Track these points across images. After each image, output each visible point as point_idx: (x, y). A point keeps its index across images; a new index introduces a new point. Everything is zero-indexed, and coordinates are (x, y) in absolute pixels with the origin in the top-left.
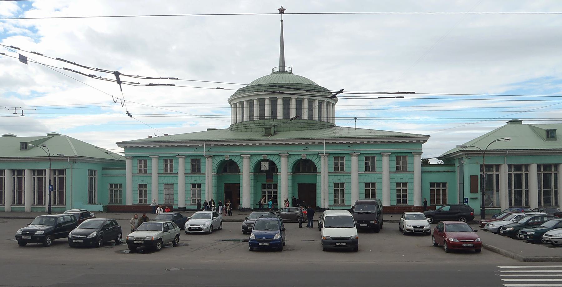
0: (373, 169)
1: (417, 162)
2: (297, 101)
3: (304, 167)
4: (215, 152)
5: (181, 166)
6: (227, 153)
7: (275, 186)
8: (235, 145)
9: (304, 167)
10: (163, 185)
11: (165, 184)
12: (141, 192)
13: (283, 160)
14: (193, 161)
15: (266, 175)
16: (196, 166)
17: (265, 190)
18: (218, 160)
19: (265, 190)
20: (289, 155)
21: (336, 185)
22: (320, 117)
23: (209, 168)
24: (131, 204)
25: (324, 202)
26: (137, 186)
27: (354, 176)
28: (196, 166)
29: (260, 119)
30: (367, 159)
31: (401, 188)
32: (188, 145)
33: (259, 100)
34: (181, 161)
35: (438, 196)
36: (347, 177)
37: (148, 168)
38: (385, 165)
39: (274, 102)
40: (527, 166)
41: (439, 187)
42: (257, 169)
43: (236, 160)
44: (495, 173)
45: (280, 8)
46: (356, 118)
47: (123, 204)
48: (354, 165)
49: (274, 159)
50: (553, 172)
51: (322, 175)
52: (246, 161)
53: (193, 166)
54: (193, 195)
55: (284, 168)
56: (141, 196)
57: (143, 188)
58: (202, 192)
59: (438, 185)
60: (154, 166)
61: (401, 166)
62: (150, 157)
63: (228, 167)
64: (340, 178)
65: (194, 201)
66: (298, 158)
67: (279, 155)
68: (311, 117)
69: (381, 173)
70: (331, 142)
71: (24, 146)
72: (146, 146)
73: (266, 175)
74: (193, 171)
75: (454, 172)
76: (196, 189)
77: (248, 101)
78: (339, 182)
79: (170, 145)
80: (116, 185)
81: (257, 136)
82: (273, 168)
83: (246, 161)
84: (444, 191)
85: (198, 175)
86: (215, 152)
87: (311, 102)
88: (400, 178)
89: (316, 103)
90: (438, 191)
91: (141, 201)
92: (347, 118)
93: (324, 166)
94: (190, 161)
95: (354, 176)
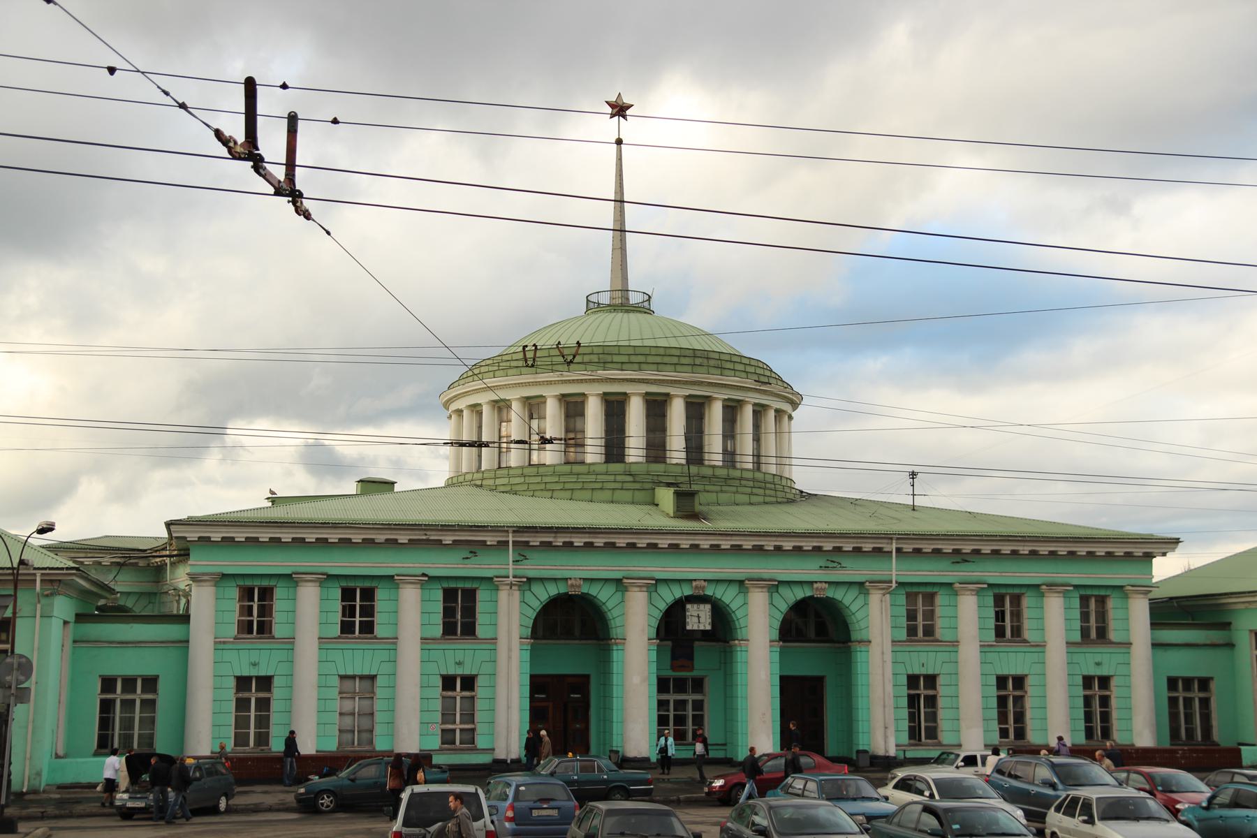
0: (1017, 631)
1: (1140, 611)
2: (724, 407)
3: (816, 625)
4: (537, 565)
5: (410, 614)
6: (576, 571)
7: (663, 685)
8: (674, 547)
9: (816, 625)
10: (335, 681)
11: (342, 677)
12: (242, 705)
14: (449, 595)
15: (693, 647)
16: (459, 612)
17: (664, 697)
19: (664, 697)
20: (775, 586)
21: (913, 680)
22: (757, 456)
23: (508, 617)
24: (314, 752)
25: (886, 737)
26: (232, 683)
27: (970, 653)
28: (459, 612)
29: (689, 461)
30: (347, 594)
31: (923, 692)
32: (448, 539)
35: (1189, 718)
36: (945, 656)
37: (992, 623)
38: (1054, 620)
41: (917, 688)
42: (671, 627)
43: (604, 595)
45: (613, 99)
46: (913, 475)
47: (381, 745)
48: (967, 617)
49: (727, 596)
51: (875, 649)
53: (448, 612)
54: (447, 716)
55: (758, 621)
56: (241, 723)
57: (254, 692)
58: (479, 705)
59: (1188, 682)
60: (309, 612)
63: (572, 620)
65: (467, 736)
66: (800, 593)
67: (291, 579)
68: (730, 456)
70: (908, 547)
72: (216, 537)
73: (693, 647)
74: (449, 629)
75: (1230, 645)
76: (458, 693)
77: (563, 398)
78: (254, 672)
79: (381, 537)
80: (129, 683)
81: (661, 513)
82: (724, 628)
84: (1205, 703)
85: (263, 644)
87: (732, 410)
88: (1095, 661)
89: (748, 412)
90: (1189, 702)
91: (241, 739)
92: (827, 462)
93: (876, 620)
95: (970, 653)
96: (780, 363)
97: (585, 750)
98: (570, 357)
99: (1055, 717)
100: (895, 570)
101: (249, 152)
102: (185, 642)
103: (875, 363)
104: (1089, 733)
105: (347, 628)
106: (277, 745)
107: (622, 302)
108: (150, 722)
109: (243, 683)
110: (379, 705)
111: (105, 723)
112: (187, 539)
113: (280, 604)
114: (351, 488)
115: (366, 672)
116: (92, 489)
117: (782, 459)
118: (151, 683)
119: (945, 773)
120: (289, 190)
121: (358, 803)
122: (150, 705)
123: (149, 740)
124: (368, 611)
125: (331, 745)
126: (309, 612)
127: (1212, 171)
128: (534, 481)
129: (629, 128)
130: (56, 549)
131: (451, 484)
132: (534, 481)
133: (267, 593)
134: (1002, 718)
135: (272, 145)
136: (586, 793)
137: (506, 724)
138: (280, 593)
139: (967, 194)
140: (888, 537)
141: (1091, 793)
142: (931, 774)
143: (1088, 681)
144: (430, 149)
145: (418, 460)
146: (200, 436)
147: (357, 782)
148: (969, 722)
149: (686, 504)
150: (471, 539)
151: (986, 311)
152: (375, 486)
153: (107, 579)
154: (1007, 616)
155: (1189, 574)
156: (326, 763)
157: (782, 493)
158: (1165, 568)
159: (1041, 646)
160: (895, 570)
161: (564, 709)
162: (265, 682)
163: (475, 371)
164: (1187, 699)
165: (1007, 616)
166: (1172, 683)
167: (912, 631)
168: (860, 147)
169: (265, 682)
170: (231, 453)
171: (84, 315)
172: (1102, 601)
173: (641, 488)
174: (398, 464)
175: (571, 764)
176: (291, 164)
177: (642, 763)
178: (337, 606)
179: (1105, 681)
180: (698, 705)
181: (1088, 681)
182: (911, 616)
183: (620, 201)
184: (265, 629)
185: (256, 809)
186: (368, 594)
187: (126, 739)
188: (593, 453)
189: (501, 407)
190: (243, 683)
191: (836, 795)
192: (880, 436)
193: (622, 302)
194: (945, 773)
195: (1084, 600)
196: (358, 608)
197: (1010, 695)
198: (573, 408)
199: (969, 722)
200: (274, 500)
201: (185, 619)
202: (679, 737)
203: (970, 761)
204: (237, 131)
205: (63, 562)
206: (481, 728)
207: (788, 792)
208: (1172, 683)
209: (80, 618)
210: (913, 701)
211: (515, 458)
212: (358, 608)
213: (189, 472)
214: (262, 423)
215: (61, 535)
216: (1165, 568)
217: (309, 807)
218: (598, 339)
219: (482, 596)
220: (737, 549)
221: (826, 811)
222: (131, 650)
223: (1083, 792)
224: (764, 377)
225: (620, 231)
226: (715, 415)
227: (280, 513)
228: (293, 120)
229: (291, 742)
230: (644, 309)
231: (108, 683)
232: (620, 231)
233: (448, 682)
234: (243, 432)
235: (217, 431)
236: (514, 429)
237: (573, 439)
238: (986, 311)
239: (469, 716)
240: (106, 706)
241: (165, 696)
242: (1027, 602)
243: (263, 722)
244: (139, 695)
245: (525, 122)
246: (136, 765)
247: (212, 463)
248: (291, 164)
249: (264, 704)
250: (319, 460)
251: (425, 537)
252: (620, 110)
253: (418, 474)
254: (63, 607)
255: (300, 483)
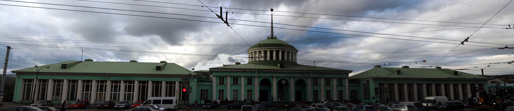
0: (329, 84)
1: (347, 81)
3: (300, 83)
4: (260, 75)
5: (243, 81)
7: (278, 92)
9: (300, 83)
13: (292, 80)
14: (248, 79)
15: (282, 87)
18: (261, 78)
22: (292, 59)
23: (256, 82)
27: (322, 87)
28: (250, 81)
33: (270, 51)
34: (243, 79)
38: (335, 82)
39: (271, 52)
40: (403, 84)
42: (279, 84)
43: (270, 79)
44: (146, 85)
47: (239, 99)
48: (322, 82)
49: (288, 79)
50: (173, 85)
51: (170, 59)
52: (275, 80)
53: (248, 81)
55: (292, 82)
57: (221, 92)
59: (354, 91)
60: (229, 81)
61: (340, 83)
62: (226, 77)
64: (316, 88)
66: (298, 79)
67: (290, 77)
68: (288, 59)
69: (226, 85)
71: (64, 66)
75: (360, 86)
77: (264, 51)
80: (205, 90)
81: (278, 67)
82: (287, 83)
83: (275, 80)
84: (356, 94)
86: (260, 75)
87: (288, 53)
88: (340, 88)
90: (204, 93)
93: (309, 83)
94: (247, 79)
95: (322, 87)
96: (294, 46)
97: (267, 100)
98: (265, 45)
99: (335, 97)
100: (312, 75)
101: (221, 17)
102: (212, 85)
103: (310, 46)
104: (340, 98)
105: (234, 83)
106: (224, 99)
107: (272, 37)
108: (207, 96)
109: (220, 91)
110: (239, 94)
111: (201, 96)
112: (213, 71)
113: (225, 80)
114: (234, 64)
115: (6, 49)
116: (200, 64)
117: (296, 59)
118: (207, 91)
119: (319, 104)
120: (226, 22)
121: (235, 107)
122: (207, 94)
123: (207, 98)
124: (237, 81)
125: (232, 99)
126: (229, 81)
127: (358, 19)
128: (260, 63)
129: (273, 13)
130: (195, 72)
131: (248, 63)
132: (260, 63)
133: (223, 78)
134: (327, 96)
135: (224, 16)
136: (267, 106)
137: (256, 96)
138: (225, 78)
139: (323, 21)
140: (311, 71)
141: (340, 107)
142: (317, 104)
143: (339, 91)
144: (247, 16)
145: (244, 59)
146: (213, 57)
147: (235, 104)
148: (323, 97)
149: (282, 66)
150: (251, 71)
151: (326, 38)
152: (238, 63)
153: (201, 76)
154: (328, 82)
155: (354, 76)
156: (231, 102)
157: (295, 64)
158: (350, 75)
159: (333, 86)
160: (312, 75)
161: (264, 95)
162: (223, 91)
163: (252, 47)
164: (353, 93)
165: (328, 82)
166: (351, 91)
167: (314, 84)
168: (307, 15)
169: (223, 91)
170: (218, 59)
171: (199, 40)
172: (341, 80)
173: (275, 63)
174: (242, 60)
175: (265, 102)
176: (227, 19)
177: (275, 102)
178: (233, 80)
179: (342, 91)
180: (284, 95)
181: (339, 91)
182: (314, 82)
183: (272, 23)
184: (223, 83)
185: (222, 108)
186: (237, 79)
187: (204, 98)
188: (268, 59)
189: (255, 52)
190: (220, 91)
191: (303, 107)
192: (312, 55)
193: (272, 37)
194: (319, 104)
195: (339, 80)
196: (236, 81)
197: (328, 94)
198: (265, 52)
199: (323, 97)
200: (224, 65)
201: (212, 82)
202: (281, 99)
203: (323, 102)
204: (219, 14)
205: (196, 74)
206: (253, 97)
207: (296, 107)
208: (351, 91)
209: (198, 81)
210: (314, 94)
211: (257, 60)
212: (236, 81)
213: (213, 61)
214: (223, 55)
215: (195, 70)
216: (350, 75)
217: (229, 108)
218: (269, 43)
219: (253, 79)
220: (289, 72)
221: (301, 109)
222: (205, 86)
223: (338, 107)
224: (292, 48)
225: (272, 27)
226: (280, 53)
227: (225, 67)
228: (227, 13)
229: (227, 99)
230: (276, 38)
231: (202, 90)
232: (272, 27)
233: (248, 91)
234: (220, 56)
235: (217, 56)
236: (257, 55)
237: (265, 56)
238: (326, 38)
239: (251, 96)
240: (202, 94)
241: (209, 92)
242: (331, 80)
243: (223, 96)
244: (206, 92)
245: (261, 12)
246: (206, 101)
247: (216, 60)
248: (227, 19)
249: (223, 94)
250: (231, 60)
251: (245, 70)
252: (272, 10)
253: (244, 62)
254: (196, 80)
255: (228, 63)
